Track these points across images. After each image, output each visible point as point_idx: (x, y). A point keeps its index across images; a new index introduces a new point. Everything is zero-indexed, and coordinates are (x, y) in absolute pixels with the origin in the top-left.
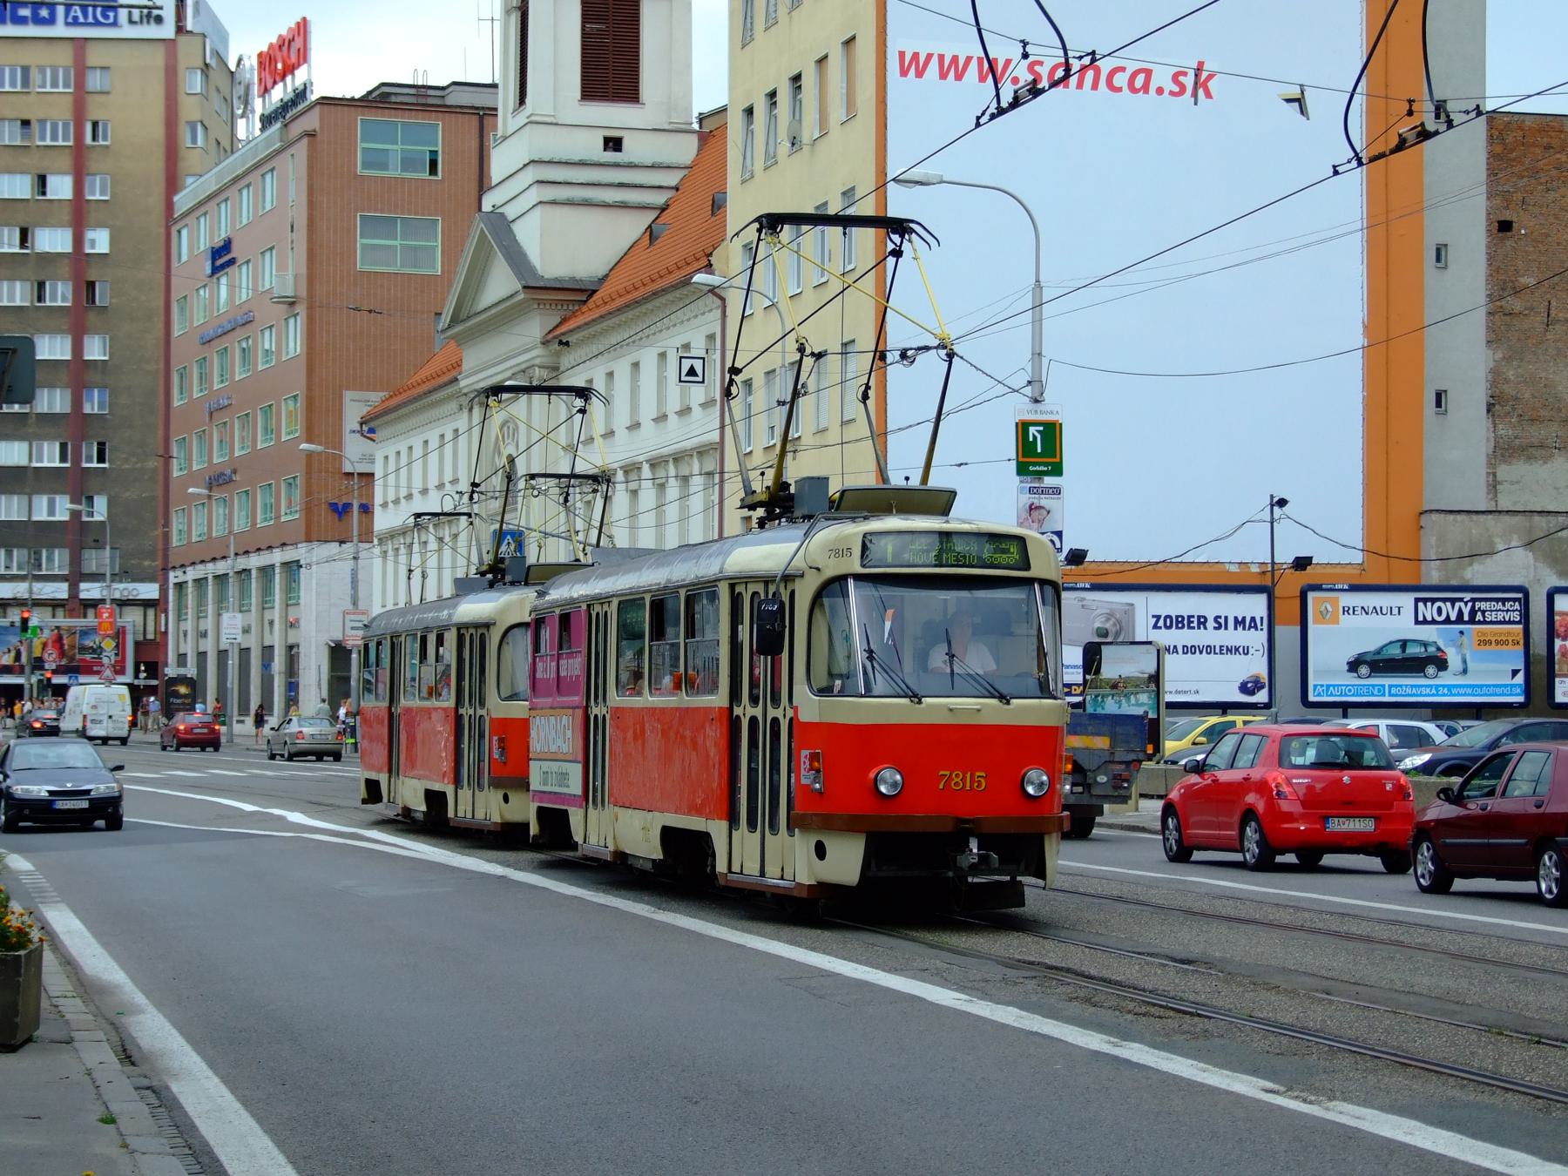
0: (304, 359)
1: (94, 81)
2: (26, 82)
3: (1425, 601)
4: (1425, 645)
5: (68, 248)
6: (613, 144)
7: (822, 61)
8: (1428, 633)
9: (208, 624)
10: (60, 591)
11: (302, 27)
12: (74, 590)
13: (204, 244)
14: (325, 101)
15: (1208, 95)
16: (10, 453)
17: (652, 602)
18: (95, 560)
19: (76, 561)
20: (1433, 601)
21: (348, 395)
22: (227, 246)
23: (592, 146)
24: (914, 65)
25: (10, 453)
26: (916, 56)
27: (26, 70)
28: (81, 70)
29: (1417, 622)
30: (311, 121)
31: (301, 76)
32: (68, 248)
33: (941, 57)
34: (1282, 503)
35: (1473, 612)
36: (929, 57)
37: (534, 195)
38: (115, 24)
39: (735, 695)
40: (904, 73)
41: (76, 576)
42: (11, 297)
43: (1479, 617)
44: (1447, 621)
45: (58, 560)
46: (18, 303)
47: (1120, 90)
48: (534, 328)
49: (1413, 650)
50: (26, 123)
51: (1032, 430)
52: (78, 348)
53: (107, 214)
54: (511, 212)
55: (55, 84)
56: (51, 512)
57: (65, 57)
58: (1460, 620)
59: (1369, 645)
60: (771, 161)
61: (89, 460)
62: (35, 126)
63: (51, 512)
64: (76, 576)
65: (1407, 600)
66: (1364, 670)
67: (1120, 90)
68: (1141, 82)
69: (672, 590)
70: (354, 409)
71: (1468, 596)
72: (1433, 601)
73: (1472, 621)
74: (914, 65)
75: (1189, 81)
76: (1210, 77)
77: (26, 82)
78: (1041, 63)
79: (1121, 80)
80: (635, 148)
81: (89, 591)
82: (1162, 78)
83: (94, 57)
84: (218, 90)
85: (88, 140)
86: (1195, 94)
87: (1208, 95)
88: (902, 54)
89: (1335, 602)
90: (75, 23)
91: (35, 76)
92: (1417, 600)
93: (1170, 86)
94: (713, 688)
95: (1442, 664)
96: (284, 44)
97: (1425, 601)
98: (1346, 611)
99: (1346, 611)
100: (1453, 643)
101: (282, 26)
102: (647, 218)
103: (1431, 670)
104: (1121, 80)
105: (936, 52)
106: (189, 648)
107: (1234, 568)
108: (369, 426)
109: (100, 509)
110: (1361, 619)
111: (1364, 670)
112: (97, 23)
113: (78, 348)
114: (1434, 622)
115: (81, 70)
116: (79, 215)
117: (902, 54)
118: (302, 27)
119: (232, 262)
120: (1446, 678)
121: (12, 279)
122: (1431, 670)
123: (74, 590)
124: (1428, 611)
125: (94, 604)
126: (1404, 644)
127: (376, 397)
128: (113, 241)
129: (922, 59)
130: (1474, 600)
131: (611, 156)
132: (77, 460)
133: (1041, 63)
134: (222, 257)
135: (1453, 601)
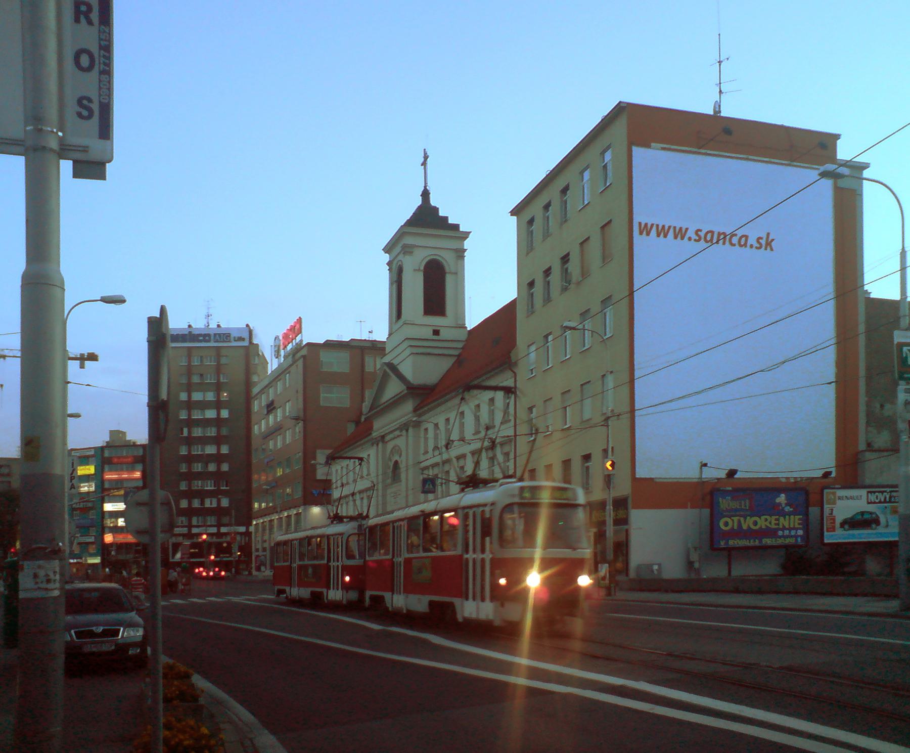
2: (202, 361)
3: (871, 492)
4: (871, 513)
6: (436, 332)
7: (547, 272)
8: (871, 508)
9: (266, 537)
11: (299, 320)
12: (219, 530)
13: (264, 403)
14: (308, 344)
15: (772, 250)
18: (225, 520)
19: (219, 520)
20: (874, 492)
21: (318, 451)
22: (272, 403)
23: (428, 333)
24: (645, 229)
26: (646, 225)
27: (201, 357)
29: (869, 503)
30: (304, 352)
31: (298, 338)
33: (658, 226)
34: (705, 465)
35: (890, 497)
36: (652, 225)
37: (408, 352)
39: (329, 560)
40: (641, 233)
43: (893, 500)
44: (880, 502)
45: (211, 520)
47: (734, 245)
48: (408, 406)
49: (866, 516)
51: (905, 349)
52: (219, 449)
54: (395, 362)
56: (211, 504)
58: (885, 502)
59: (848, 515)
60: (547, 299)
63: (211, 504)
64: (219, 526)
65: (863, 492)
66: (846, 527)
67: (734, 245)
68: (743, 242)
70: (321, 457)
71: (888, 490)
72: (874, 492)
73: (890, 502)
74: (645, 229)
75: (763, 242)
76: (773, 240)
77: (202, 361)
78: (700, 230)
79: (735, 240)
80: (445, 334)
81: (224, 530)
82: (752, 241)
83: (223, 352)
86: (766, 249)
87: (772, 250)
88: (640, 224)
89: (834, 494)
92: (868, 492)
93: (756, 244)
94: (323, 558)
95: (877, 522)
96: (292, 328)
97: (871, 492)
98: (840, 498)
99: (840, 498)
100: (885, 513)
101: (291, 322)
102: (454, 359)
103: (874, 526)
104: (735, 240)
105: (655, 223)
106: (259, 546)
107: (784, 480)
108: (331, 459)
109: (225, 502)
110: (850, 502)
111: (846, 527)
113: (219, 449)
114: (875, 503)
117: (640, 224)
118: (299, 320)
119: (274, 408)
120: (880, 530)
122: (874, 526)
124: (872, 498)
125: (226, 534)
126: (862, 513)
127: (329, 452)
128: (230, 414)
129: (649, 226)
130: (891, 492)
131: (435, 337)
133: (700, 230)
134: (271, 407)
135: (882, 492)
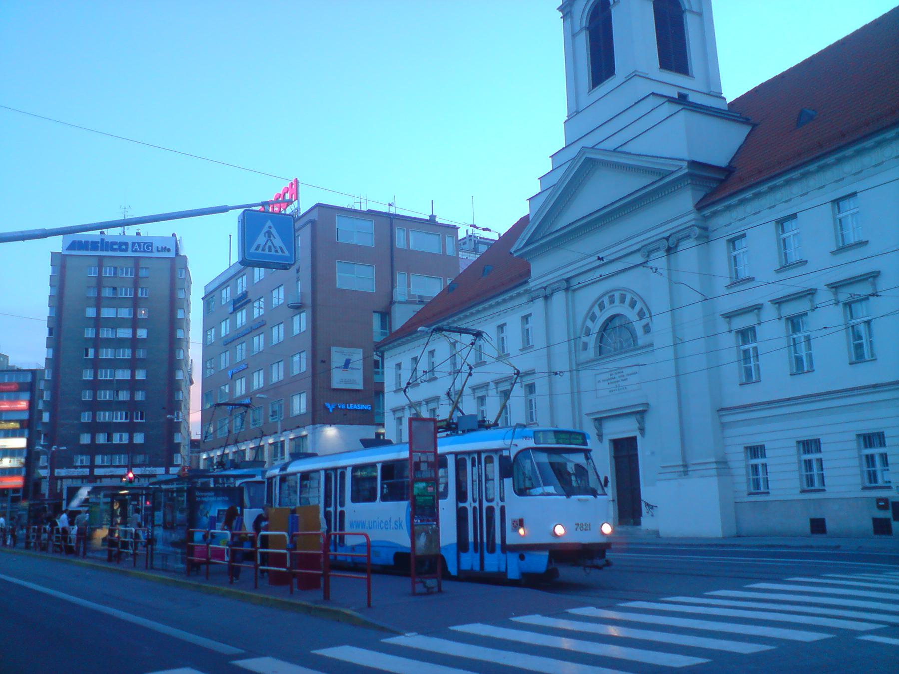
0: (309, 374)
1: (143, 273)
2: (115, 273)
5: (130, 336)
10: (86, 472)
12: (92, 472)
16: (6, 426)
17: (382, 468)
25: (6, 426)
27: (115, 268)
28: (137, 268)
32: (130, 336)
38: (152, 251)
41: (92, 467)
42: (107, 355)
46: (109, 357)
50: (115, 288)
52: (133, 375)
53: (144, 323)
55: (127, 274)
57: (131, 263)
61: (137, 419)
62: (119, 289)
69: (335, 469)
81: (98, 472)
83: (142, 263)
84: (298, 271)
85: (140, 295)
90: (136, 251)
91: (119, 272)
112: (145, 251)
113: (133, 375)
115: (137, 268)
116: (135, 323)
121: (107, 348)
123: (92, 472)
132: (132, 419)
